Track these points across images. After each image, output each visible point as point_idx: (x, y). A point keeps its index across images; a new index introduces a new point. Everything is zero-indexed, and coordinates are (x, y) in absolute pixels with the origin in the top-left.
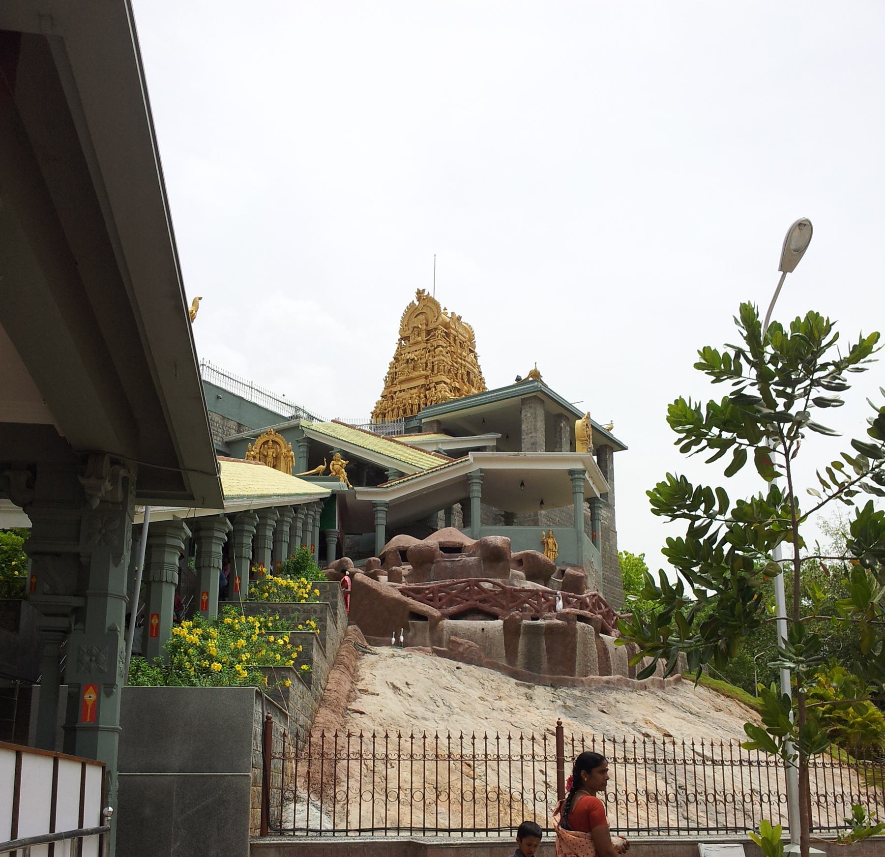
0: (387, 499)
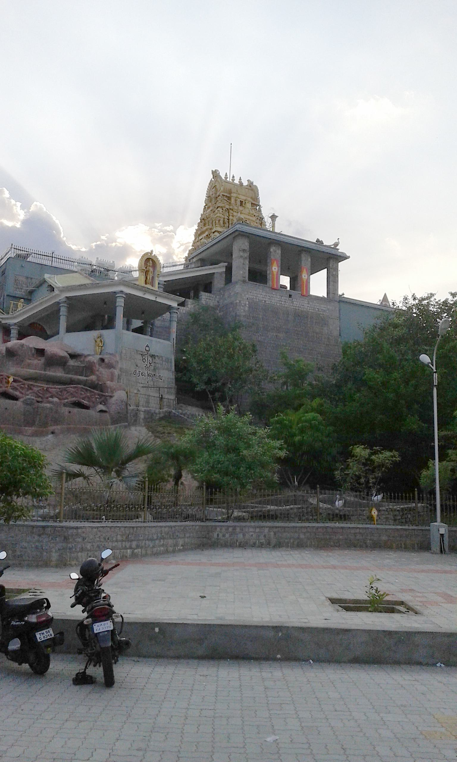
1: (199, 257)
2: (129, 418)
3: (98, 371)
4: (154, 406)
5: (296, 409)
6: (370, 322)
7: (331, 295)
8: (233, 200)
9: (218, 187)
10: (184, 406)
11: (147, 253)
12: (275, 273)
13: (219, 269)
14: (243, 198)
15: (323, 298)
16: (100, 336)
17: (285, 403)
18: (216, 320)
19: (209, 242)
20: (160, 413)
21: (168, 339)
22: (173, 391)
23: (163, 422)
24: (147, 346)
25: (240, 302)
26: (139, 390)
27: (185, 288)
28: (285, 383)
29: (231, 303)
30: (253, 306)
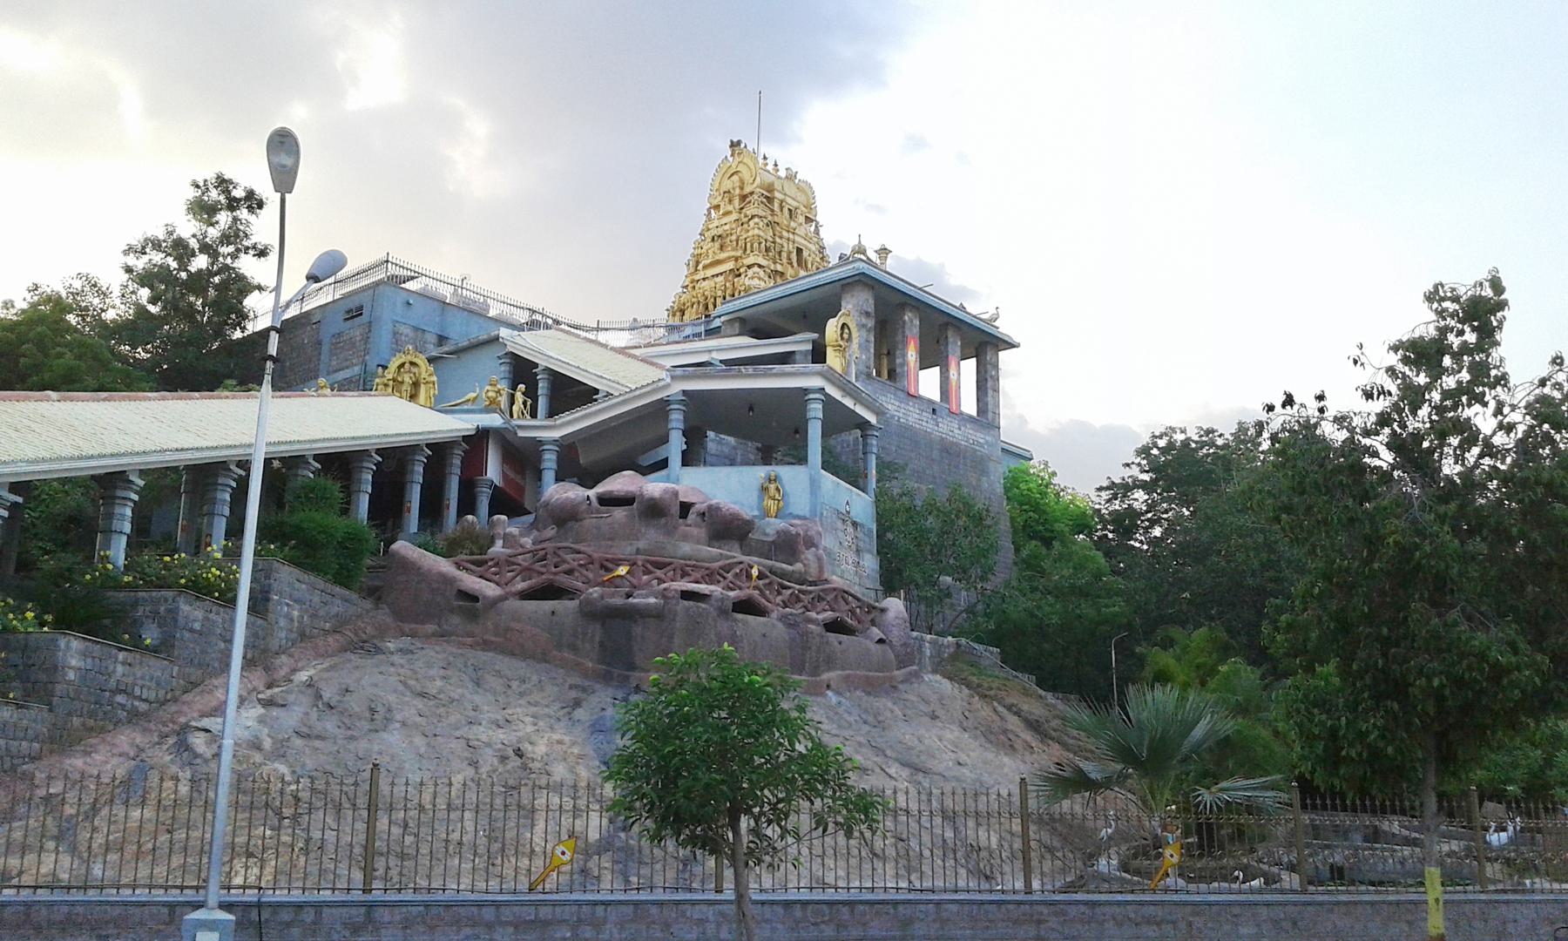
0: (557, 434)
15: (971, 417)
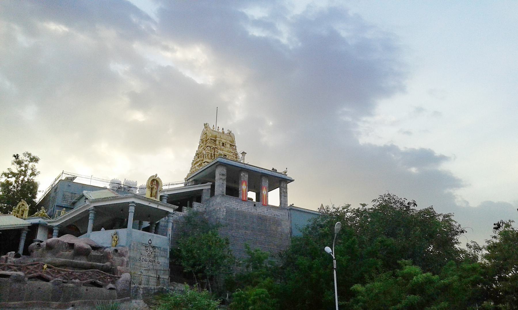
1: (195, 179)
2: (131, 293)
3: (112, 259)
4: (153, 285)
5: (254, 286)
6: (304, 222)
7: (283, 205)
8: (217, 143)
9: (208, 134)
10: (176, 283)
11: (153, 176)
12: (244, 190)
13: (207, 187)
14: (224, 141)
15: (278, 207)
16: (116, 234)
17: (247, 281)
18: (203, 222)
19: (201, 169)
20: (154, 290)
21: (166, 235)
22: (168, 272)
23: (157, 296)
24: (150, 240)
25: (220, 209)
26: (141, 272)
27: (180, 200)
28: (248, 267)
29: (214, 210)
30: (229, 212)
